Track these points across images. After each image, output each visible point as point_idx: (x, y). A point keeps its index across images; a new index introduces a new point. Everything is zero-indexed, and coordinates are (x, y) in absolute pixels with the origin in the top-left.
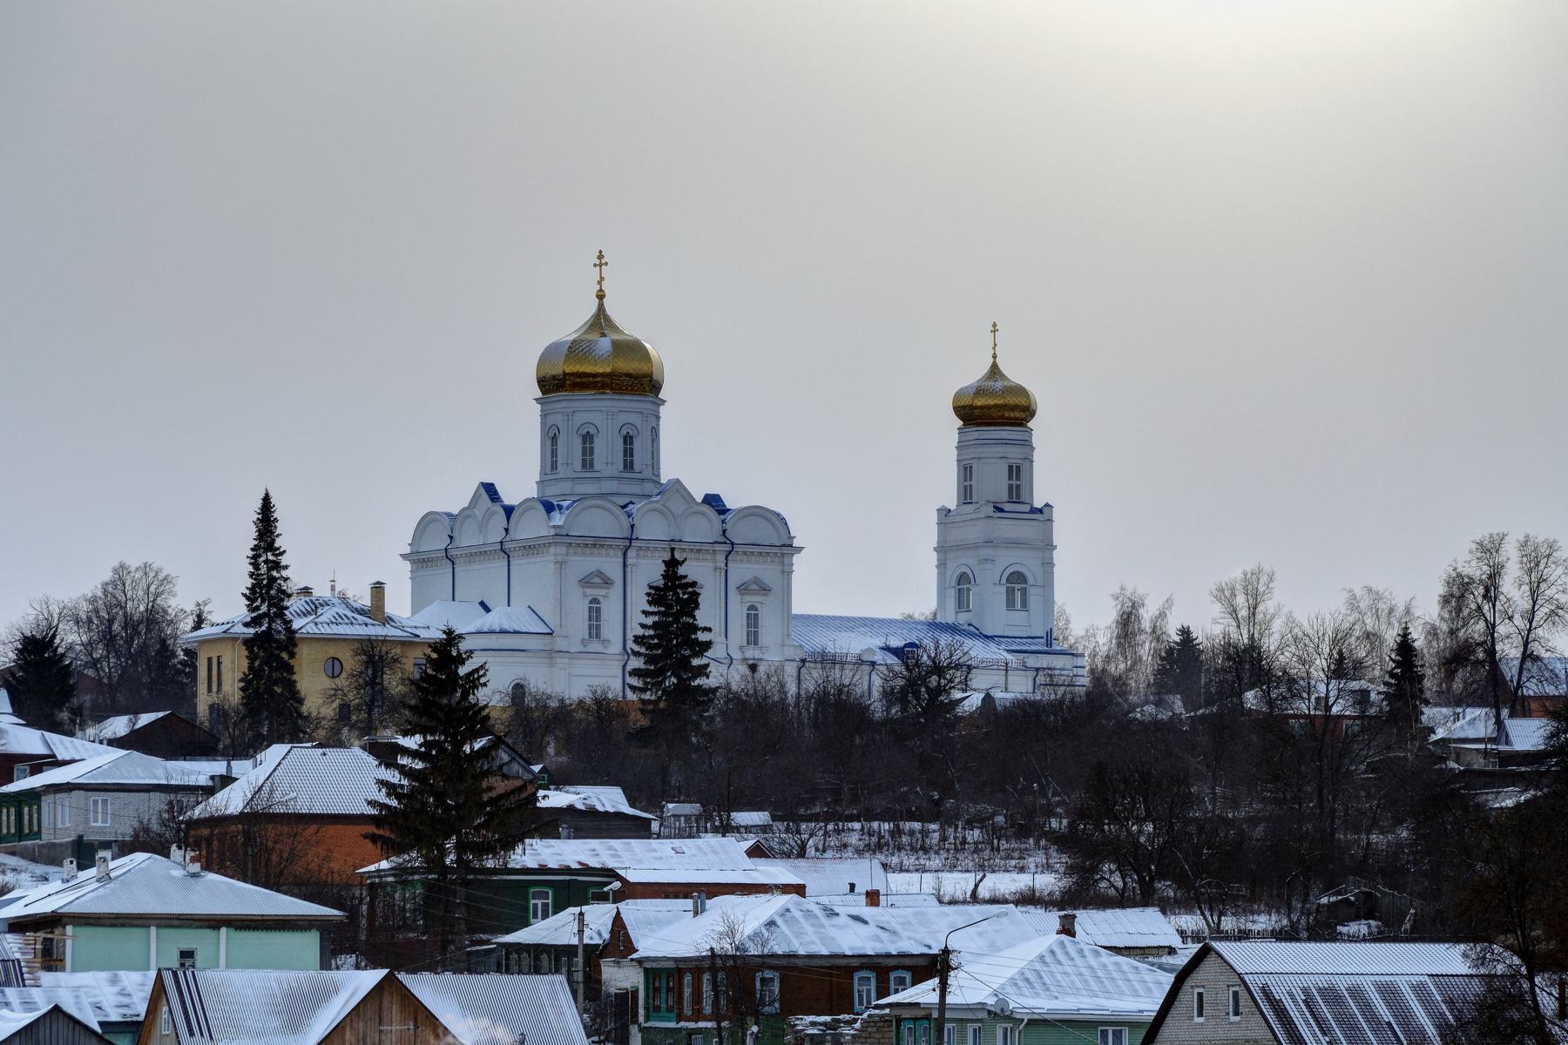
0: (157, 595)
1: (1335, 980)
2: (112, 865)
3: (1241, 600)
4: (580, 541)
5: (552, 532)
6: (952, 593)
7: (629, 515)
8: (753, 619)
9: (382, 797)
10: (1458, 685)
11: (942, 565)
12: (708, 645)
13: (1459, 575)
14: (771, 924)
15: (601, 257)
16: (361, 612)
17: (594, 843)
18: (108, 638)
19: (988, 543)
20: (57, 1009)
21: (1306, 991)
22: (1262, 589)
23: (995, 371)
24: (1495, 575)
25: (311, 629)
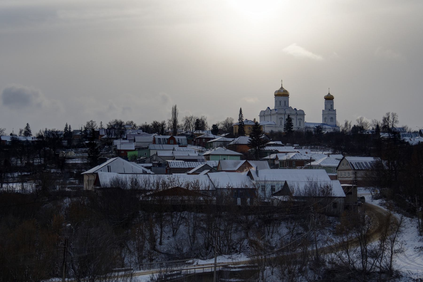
0: (232, 121)
1: (359, 161)
2: (216, 149)
3: (359, 121)
4: (279, 114)
5: (276, 113)
6: (324, 120)
7: (285, 111)
8: (300, 123)
9: (249, 141)
10: (384, 130)
11: (323, 117)
12: (293, 125)
13: (384, 117)
14: (294, 156)
15: (282, 80)
16: (253, 122)
17: (275, 147)
18: (226, 126)
20: (206, 164)
21: (356, 163)
22: (362, 119)
24: (389, 117)
25: (247, 124)
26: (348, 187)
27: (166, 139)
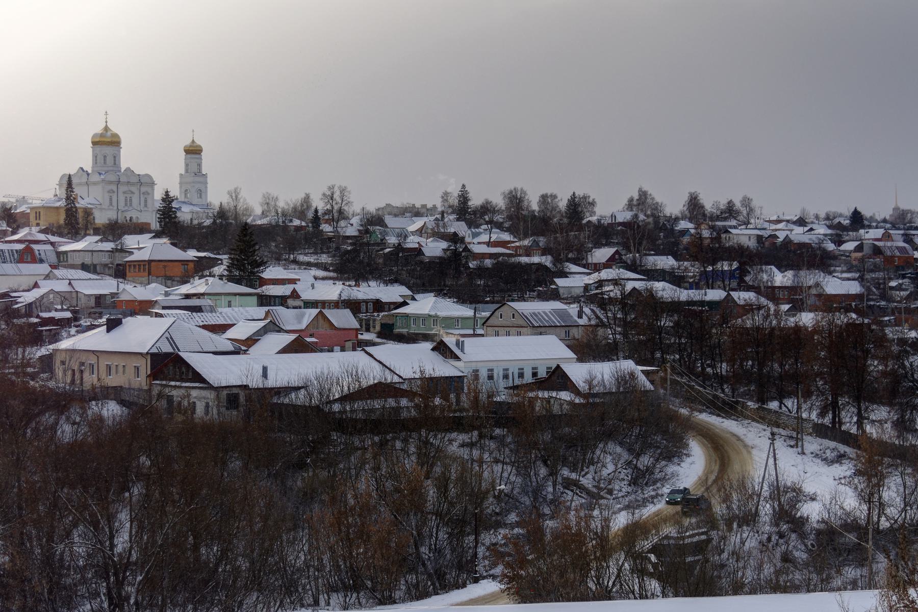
3: (234, 195)
8: (146, 201)
11: (181, 187)
19: (193, 182)
23: (193, 141)
26: (652, 372)
27: (15, 251)
